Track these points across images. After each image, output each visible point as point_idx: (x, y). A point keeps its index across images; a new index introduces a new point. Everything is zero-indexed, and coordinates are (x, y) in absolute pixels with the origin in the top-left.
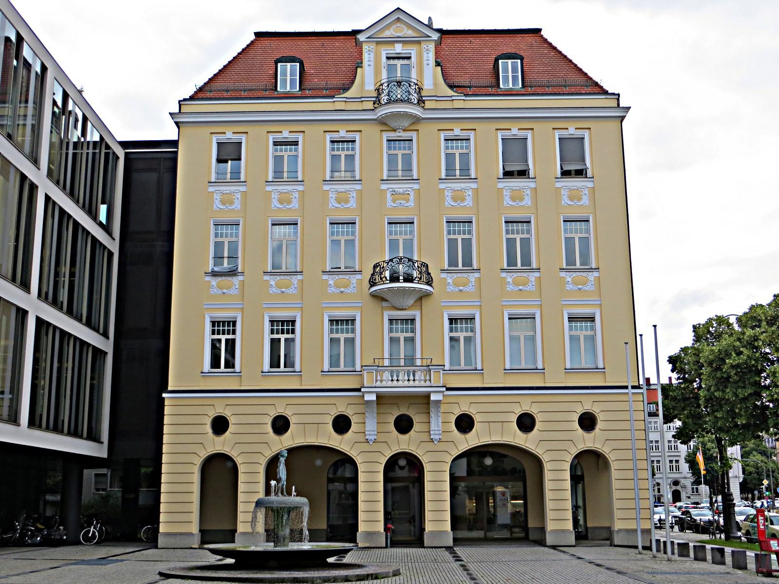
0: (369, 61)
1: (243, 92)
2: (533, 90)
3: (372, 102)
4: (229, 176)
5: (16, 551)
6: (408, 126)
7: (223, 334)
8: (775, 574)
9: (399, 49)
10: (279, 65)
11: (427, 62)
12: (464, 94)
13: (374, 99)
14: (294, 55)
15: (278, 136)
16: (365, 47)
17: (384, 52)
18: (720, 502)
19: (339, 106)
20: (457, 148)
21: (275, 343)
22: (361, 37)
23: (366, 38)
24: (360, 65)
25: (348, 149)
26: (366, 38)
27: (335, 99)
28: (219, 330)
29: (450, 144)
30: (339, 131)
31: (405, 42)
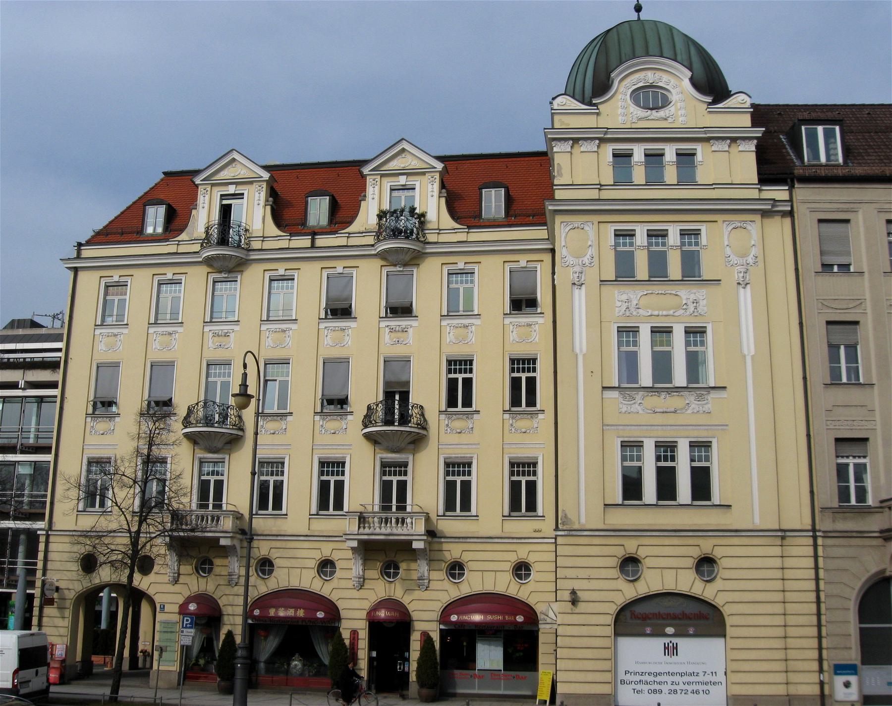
0: (433, 191)
1: (135, 235)
2: (535, 220)
3: (200, 244)
4: (168, 316)
5: (148, 699)
6: (234, 267)
7: (333, 475)
8: (821, 675)
9: (402, 180)
10: (484, 191)
11: (372, 196)
12: (468, 226)
13: (375, 234)
14: (500, 181)
15: (331, 271)
16: (369, 180)
17: (387, 183)
18: (276, 612)
19: (342, 241)
20: (462, 282)
21: (842, 471)
22: (366, 170)
23: (369, 171)
24: (195, 207)
25: (467, 282)
26: (369, 171)
27: (337, 235)
28: (272, 472)
29: (454, 278)
30: (277, 270)
31: (409, 174)
